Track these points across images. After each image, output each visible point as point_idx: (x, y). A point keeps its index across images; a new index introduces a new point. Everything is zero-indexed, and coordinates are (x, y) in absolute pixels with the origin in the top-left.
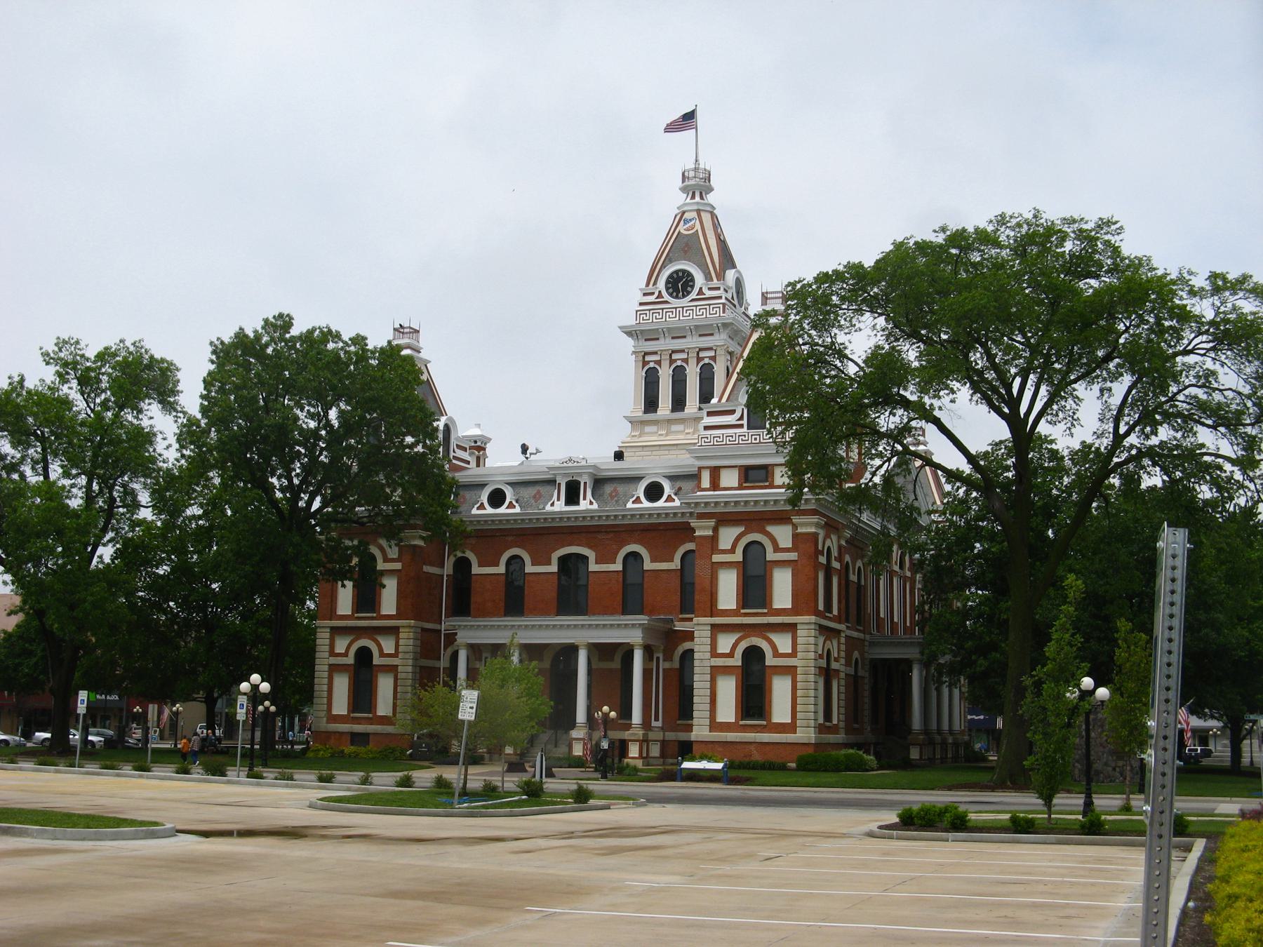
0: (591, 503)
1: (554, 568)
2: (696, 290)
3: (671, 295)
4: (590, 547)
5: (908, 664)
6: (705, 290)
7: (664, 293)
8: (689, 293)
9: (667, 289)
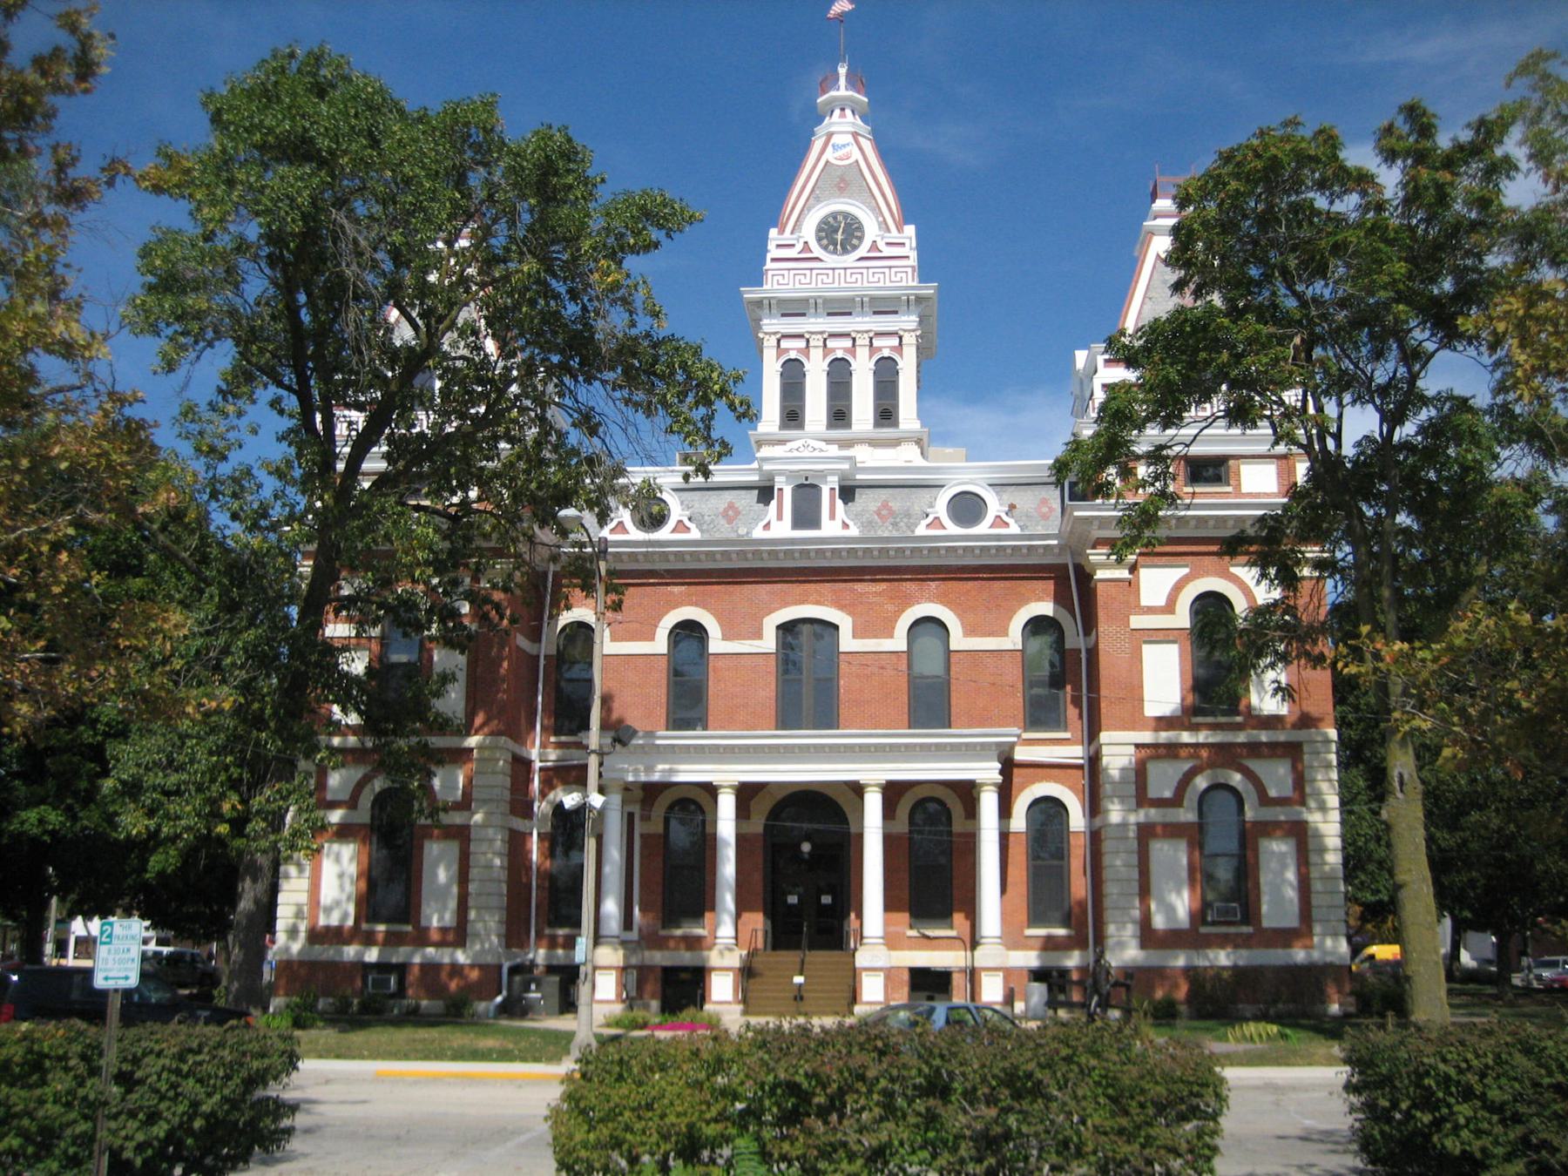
0: (845, 526)
2: (866, 244)
3: (825, 248)
4: (841, 607)
5: (967, 792)
6: (881, 245)
7: (813, 244)
8: (855, 248)
9: (819, 240)
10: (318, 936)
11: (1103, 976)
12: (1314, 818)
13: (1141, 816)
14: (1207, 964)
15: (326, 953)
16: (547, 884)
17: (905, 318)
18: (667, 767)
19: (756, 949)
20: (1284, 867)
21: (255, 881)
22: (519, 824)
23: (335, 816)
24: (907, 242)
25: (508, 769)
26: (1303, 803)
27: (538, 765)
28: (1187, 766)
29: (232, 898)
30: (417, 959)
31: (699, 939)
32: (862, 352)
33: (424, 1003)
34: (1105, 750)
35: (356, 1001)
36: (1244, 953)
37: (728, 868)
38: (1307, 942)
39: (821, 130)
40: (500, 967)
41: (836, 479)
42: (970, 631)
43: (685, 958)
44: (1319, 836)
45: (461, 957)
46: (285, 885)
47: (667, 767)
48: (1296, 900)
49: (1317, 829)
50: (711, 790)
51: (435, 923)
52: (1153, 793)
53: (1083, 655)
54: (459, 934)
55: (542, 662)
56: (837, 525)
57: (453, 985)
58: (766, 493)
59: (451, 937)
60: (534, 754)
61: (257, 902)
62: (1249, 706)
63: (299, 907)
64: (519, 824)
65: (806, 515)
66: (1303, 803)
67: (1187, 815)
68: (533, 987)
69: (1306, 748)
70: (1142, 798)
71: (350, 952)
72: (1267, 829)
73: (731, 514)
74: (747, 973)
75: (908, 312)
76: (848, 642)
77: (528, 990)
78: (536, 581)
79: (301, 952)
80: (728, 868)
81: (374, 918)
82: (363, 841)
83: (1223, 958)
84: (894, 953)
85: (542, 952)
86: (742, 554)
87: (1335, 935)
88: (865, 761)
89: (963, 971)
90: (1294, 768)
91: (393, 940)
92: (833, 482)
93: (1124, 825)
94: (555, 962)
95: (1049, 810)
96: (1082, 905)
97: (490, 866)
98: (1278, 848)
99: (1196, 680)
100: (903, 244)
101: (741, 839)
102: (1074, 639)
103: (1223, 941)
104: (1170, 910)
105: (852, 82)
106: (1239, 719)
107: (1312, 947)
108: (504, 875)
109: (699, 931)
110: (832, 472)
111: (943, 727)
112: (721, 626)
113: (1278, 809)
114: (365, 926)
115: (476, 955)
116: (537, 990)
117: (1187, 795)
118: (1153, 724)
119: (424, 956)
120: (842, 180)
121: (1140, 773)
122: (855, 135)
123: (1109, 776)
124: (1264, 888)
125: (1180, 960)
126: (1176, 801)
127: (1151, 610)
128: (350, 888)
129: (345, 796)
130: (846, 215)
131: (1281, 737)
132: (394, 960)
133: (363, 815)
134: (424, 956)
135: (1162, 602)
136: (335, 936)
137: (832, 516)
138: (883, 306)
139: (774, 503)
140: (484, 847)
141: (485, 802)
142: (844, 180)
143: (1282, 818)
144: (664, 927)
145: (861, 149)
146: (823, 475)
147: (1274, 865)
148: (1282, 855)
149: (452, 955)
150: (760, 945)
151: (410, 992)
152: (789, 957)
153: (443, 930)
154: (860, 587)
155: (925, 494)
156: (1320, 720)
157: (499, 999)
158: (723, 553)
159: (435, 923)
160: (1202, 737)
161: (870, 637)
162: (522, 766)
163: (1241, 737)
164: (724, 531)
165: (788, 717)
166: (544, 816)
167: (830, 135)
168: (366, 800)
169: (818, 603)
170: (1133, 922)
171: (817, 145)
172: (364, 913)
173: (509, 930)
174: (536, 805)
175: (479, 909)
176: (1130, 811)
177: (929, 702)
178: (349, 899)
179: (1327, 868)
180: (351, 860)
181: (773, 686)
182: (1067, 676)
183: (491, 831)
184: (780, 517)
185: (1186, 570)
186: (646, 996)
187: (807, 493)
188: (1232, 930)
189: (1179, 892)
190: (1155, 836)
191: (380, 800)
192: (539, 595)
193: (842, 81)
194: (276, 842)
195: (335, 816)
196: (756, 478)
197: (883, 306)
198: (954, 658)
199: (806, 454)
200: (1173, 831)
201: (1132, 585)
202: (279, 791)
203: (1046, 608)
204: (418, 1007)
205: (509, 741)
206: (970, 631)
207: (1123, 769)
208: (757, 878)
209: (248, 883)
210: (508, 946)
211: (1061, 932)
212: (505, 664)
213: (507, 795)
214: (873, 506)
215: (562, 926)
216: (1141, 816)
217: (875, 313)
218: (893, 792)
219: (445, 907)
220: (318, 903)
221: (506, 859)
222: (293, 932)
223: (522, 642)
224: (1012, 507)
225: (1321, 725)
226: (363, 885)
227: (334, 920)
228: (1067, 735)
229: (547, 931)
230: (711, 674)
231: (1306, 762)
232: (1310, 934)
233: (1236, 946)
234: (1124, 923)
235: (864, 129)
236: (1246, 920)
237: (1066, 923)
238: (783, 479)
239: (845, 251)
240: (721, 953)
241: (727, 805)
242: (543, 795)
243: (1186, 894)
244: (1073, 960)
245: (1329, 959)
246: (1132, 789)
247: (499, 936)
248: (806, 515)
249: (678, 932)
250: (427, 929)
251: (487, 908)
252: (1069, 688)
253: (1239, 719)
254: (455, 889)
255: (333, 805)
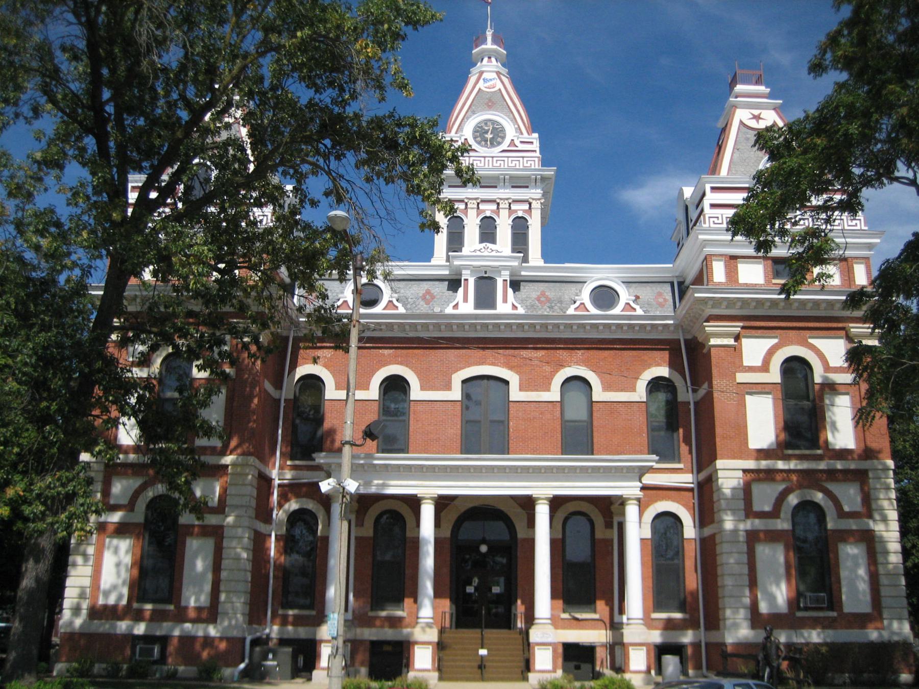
0: (515, 307)
1: (455, 394)
3: (479, 143)
4: (511, 368)
6: (517, 142)
8: (499, 144)
9: (475, 138)
10: (96, 613)
11: (774, 651)
12: (878, 527)
13: (748, 525)
14: (803, 641)
15: (103, 627)
16: (280, 575)
17: (534, 191)
18: (381, 482)
19: (445, 628)
20: (857, 565)
21: (37, 561)
22: (262, 527)
23: (116, 517)
24: (534, 141)
25: (255, 483)
26: (870, 516)
27: (277, 482)
28: (781, 487)
29: (18, 576)
30: (177, 633)
31: (400, 619)
32: (504, 213)
33: (181, 668)
34: (720, 474)
35: (125, 666)
36: (830, 632)
37: (428, 562)
38: (879, 625)
39: (475, 71)
40: (244, 639)
41: (508, 273)
42: (607, 387)
43: (388, 634)
44: (883, 542)
45: (212, 631)
46: (72, 572)
47: (381, 482)
48: (868, 591)
49: (881, 537)
50: (414, 503)
51: (192, 603)
52: (756, 508)
53: (692, 407)
54: (211, 613)
55: (283, 404)
56: (507, 305)
57: (205, 655)
58: (454, 283)
59: (204, 615)
60: (274, 474)
61: (38, 580)
62: (826, 442)
63: (83, 588)
64: (262, 527)
65: (486, 297)
66: (870, 516)
67: (783, 524)
68: (271, 656)
69: (871, 475)
70: (749, 512)
71: (123, 626)
72: (844, 536)
73: (428, 297)
74: (440, 646)
75: (536, 187)
76: (515, 394)
77: (266, 658)
78: (280, 342)
79: (82, 626)
80: (428, 562)
81: (143, 599)
82: (137, 537)
83: (815, 636)
84: (560, 632)
85: (276, 628)
86: (437, 326)
87: (900, 619)
88: (537, 480)
89: (604, 645)
90: (862, 490)
91: (158, 617)
92: (506, 275)
93: (735, 531)
94: (285, 636)
95: (667, 524)
96: (694, 595)
97: (238, 558)
98: (851, 552)
99: (786, 422)
100: (532, 143)
101: (438, 542)
102: (685, 395)
103: (814, 623)
104: (772, 599)
105: (495, 41)
106: (819, 452)
107: (883, 629)
108: (249, 566)
109: (399, 613)
110: (505, 268)
111: (588, 454)
112: (420, 379)
113: (851, 521)
114: (135, 605)
115: (224, 629)
116: (273, 659)
117: (784, 509)
118: (755, 454)
119: (182, 630)
120: (490, 100)
121: (747, 490)
122: (498, 73)
123: (723, 494)
124: (844, 583)
125: (782, 637)
126: (774, 514)
127: (751, 369)
128: (125, 575)
129: (124, 501)
130: (494, 122)
131: (852, 466)
132: (158, 633)
133: (139, 516)
134: (182, 630)
135: (759, 363)
136: (111, 613)
137: (505, 300)
138: (519, 182)
139: (461, 290)
140: (234, 543)
141: (237, 507)
142: (491, 101)
143: (854, 527)
144: (372, 610)
145: (503, 83)
146: (498, 270)
147: (849, 563)
148: (855, 557)
149: (205, 630)
150: (447, 624)
151: (170, 660)
152: (471, 634)
153: (199, 609)
154: (524, 353)
155: (573, 288)
156: (879, 452)
157: (242, 666)
158: (423, 325)
159: (192, 603)
160: (792, 465)
161: (532, 390)
162: (265, 481)
163: (822, 465)
164: (423, 308)
165: (470, 445)
166: (281, 521)
167: (481, 73)
168: (141, 505)
169: (493, 364)
170: (745, 607)
171: (472, 80)
172: (135, 594)
173: (251, 610)
174: (275, 512)
175: (228, 592)
176: (740, 521)
177: (578, 437)
178: (124, 583)
179: (891, 566)
180: (127, 552)
181: (459, 426)
182: (686, 418)
183: (240, 530)
184: (466, 300)
185: (775, 341)
186: (357, 664)
187: (485, 283)
188: (821, 614)
189: (778, 585)
190: (759, 540)
191: (152, 504)
192: (280, 355)
193: (489, 39)
194: (52, 524)
195: (116, 517)
196: (447, 272)
197: (519, 182)
198: (596, 407)
199: (486, 253)
200: (773, 536)
201: (736, 350)
202: (59, 479)
203: (663, 371)
204: (176, 671)
205: (257, 461)
206: (607, 387)
207: (733, 489)
208: (446, 571)
209: (31, 563)
210: (250, 622)
211: (678, 615)
212: (256, 401)
213: (254, 503)
214: (534, 295)
215: (292, 608)
216: (748, 525)
217: (513, 187)
218: (556, 503)
219: (201, 591)
220: (99, 588)
221: (251, 553)
222: (76, 610)
223: (268, 386)
224: (637, 297)
225: (880, 456)
226: (136, 572)
227: (112, 600)
228: (681, 466)
229: (280, 612)
230: (412, 416)
231: (872, 486)
232: (880, 618)
233: (824, 627)
234: (738, 608)
235: (504, 71)
236: (831, 607)
237: (682, 608)
238: (468, 272)
239: (492, 145)
240: (423, 629)
241: (428, 513)
242: (280, 506)
243: (783, 586)
244: (687, 638)
245: (896, 638)
246: (741, 504)
247: (243, 614)
248: (486, 297)
249: (384, 614)
250: (186, 608)
251: (236, 592)
252: (681, 431)
253: (819, 452)
254: (210, 576)
255: (114, 508)
